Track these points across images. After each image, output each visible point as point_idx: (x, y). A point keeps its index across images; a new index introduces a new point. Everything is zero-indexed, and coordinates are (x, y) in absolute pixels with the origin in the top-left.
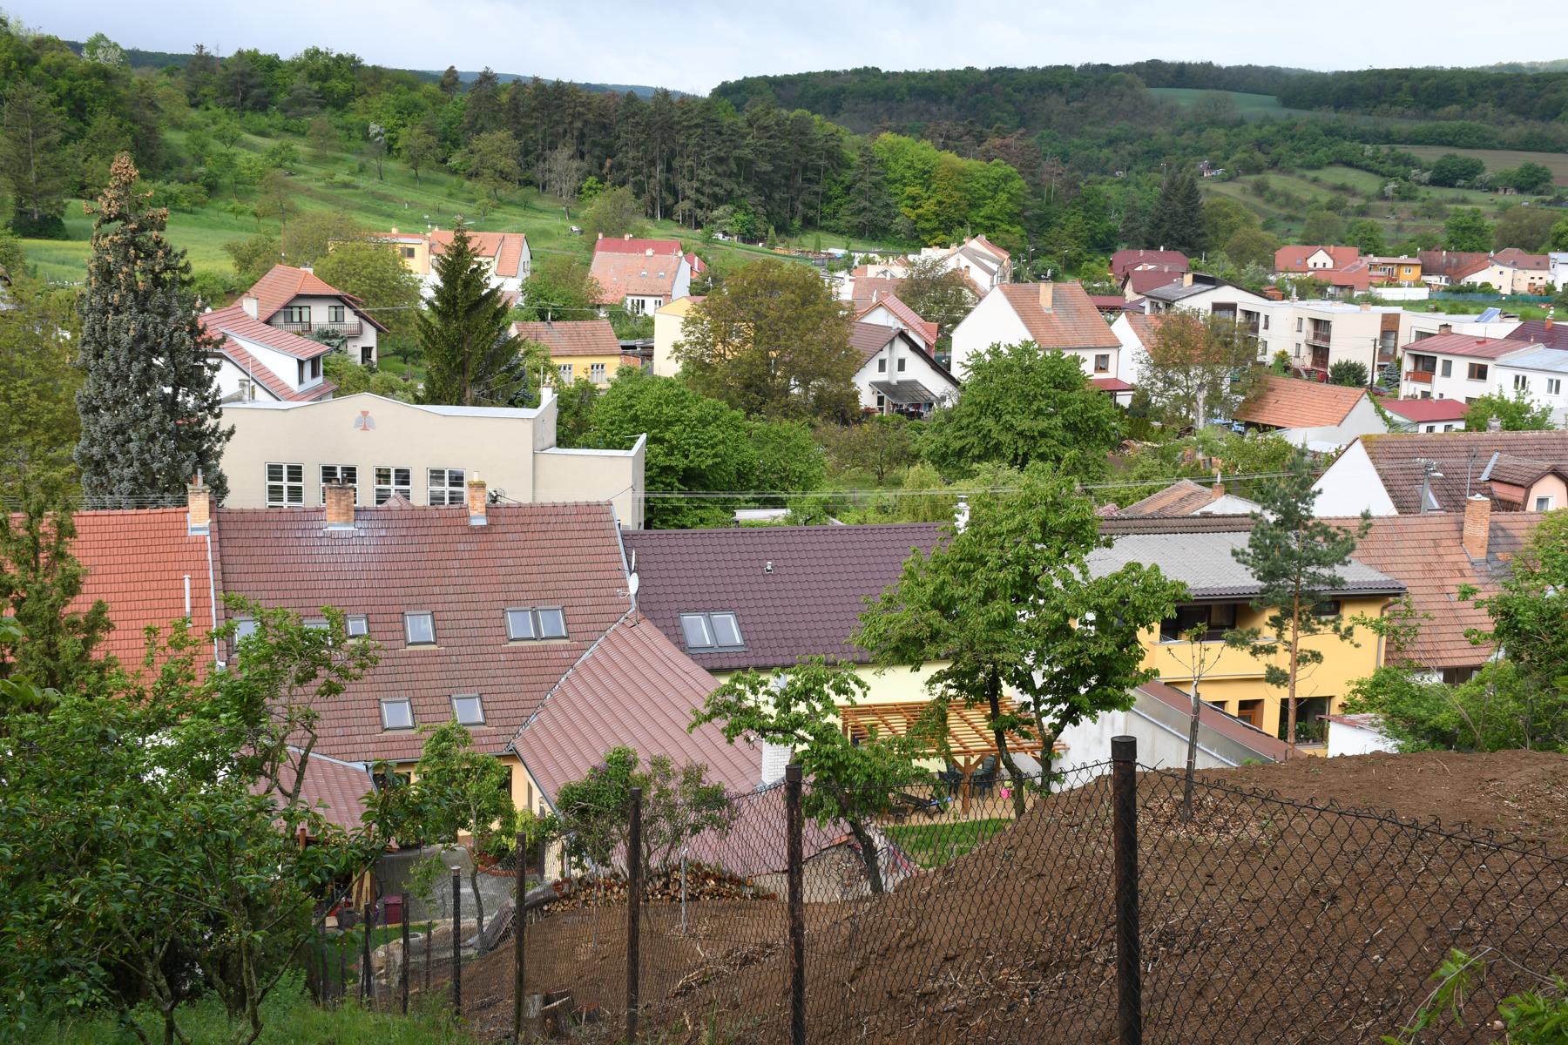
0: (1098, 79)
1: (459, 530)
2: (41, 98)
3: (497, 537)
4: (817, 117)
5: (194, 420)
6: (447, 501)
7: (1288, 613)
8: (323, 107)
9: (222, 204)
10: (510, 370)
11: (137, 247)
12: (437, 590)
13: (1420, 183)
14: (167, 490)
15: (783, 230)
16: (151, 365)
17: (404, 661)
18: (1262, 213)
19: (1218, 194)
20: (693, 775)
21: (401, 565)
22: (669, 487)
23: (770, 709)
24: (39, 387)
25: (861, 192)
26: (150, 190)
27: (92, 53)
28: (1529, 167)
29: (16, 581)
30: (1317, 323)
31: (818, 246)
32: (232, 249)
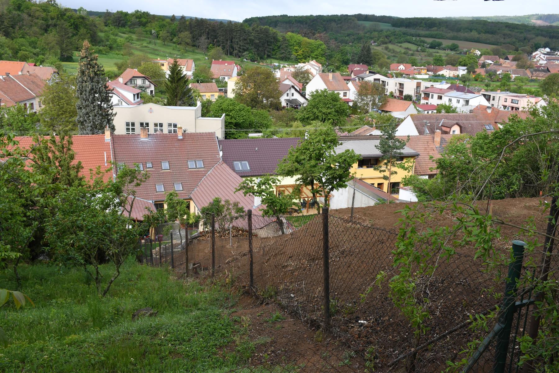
0: (345, 18)
1: (175, 140)
2: (66, 25)
3: (185, 142)
4: (271, 28)
5: (106, 111)
6: (173, 132)
7: (389, 162)
8: (140, 26)
9: (113, 52)
10: (189, 96)
11: (90, 65)
12: (170, 156)
13: (427, 48)
14: (100, 129)
15: (262, 58)
16: (95, 96)
17: (161, 174)
18: (387, 55)
19: (376, 50)
20: (236, 204)
21: (160, 149)
22: (231, 128)
23: (256, 188)
24: (67, 102)
25: (282, 48)
26: (95, 48)
27: (80, 12)
28: (453, 44)
29: (58, 156)
30: (400, 84)
31: (271, 62)
32: (116, 64)
